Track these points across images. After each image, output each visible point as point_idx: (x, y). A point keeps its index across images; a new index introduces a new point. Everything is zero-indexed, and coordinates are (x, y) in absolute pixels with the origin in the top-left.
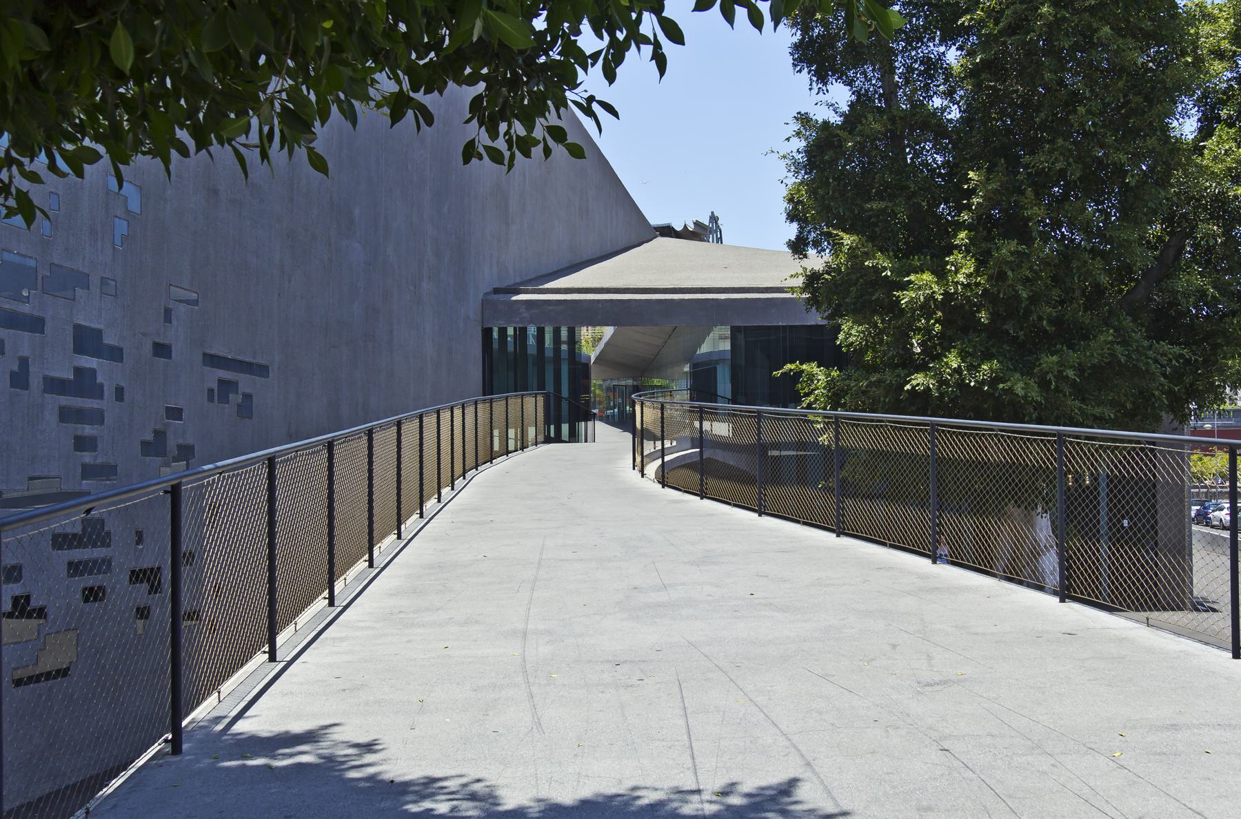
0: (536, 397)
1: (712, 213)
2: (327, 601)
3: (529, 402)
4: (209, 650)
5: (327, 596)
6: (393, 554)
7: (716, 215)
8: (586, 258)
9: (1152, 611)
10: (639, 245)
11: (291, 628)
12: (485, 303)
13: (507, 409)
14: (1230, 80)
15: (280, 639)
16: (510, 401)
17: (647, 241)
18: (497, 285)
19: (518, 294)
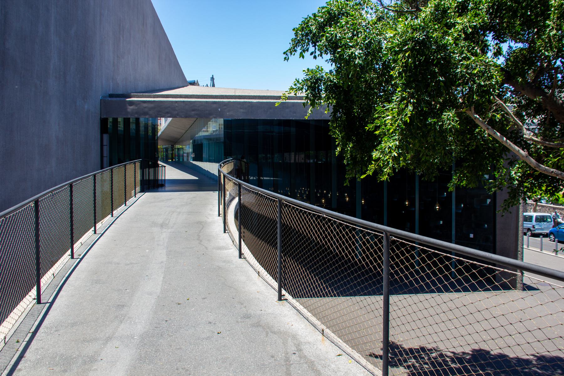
0: (135, 164)
1: (213, 75)
2: (70, 256)
3: (130, 167)
4: (14, 243)
5: (70, 254)
6: (105, 230)
7: (214, 77)
8: (161, 88)
9: (325, 297)
10: (183, 87)
11: (116, 211)
12: (103, 102)
13: (112, 177)
14: (306, 38)
15: (114, 212)
16: (114, 170)
17: (186, 86)
18: (111, 92)
19: (130, 98)
